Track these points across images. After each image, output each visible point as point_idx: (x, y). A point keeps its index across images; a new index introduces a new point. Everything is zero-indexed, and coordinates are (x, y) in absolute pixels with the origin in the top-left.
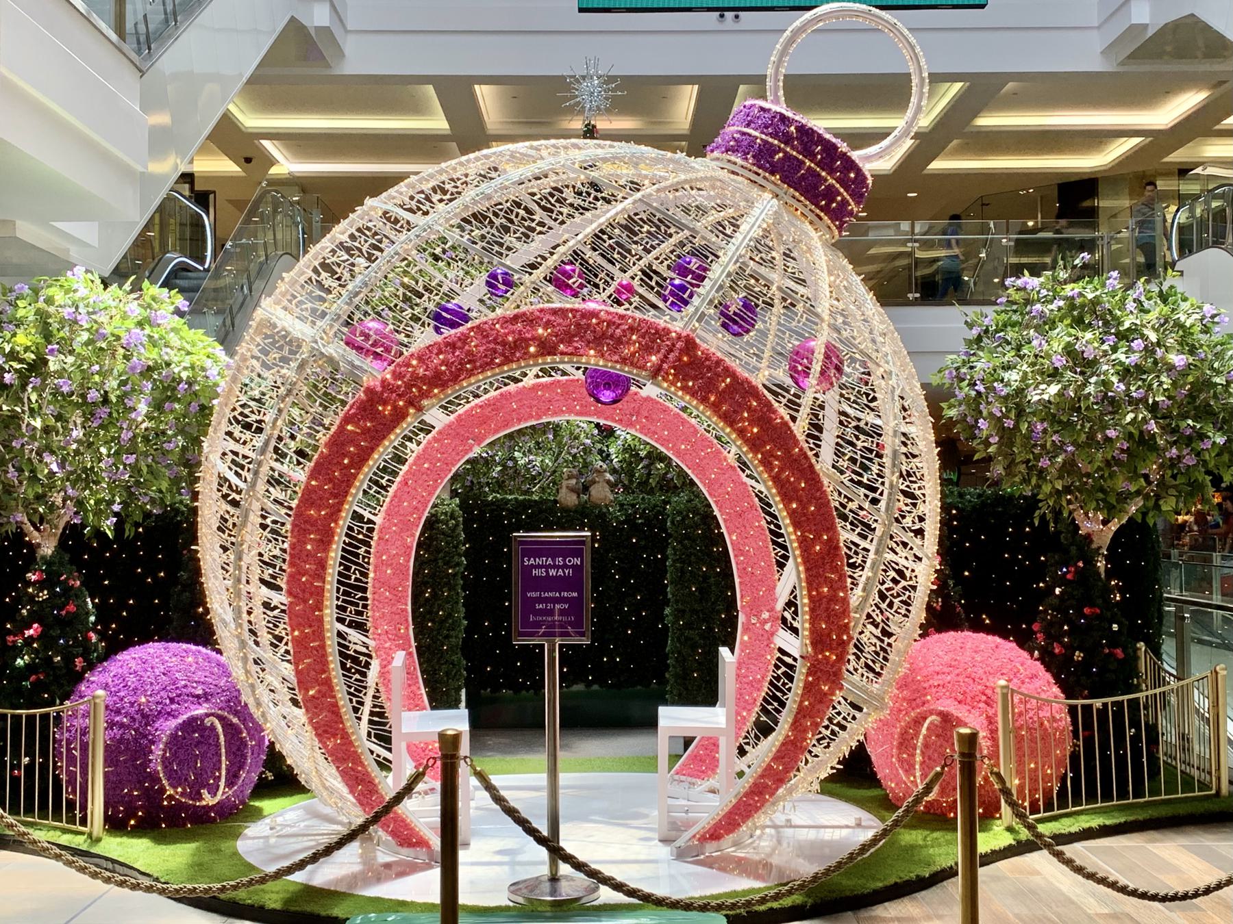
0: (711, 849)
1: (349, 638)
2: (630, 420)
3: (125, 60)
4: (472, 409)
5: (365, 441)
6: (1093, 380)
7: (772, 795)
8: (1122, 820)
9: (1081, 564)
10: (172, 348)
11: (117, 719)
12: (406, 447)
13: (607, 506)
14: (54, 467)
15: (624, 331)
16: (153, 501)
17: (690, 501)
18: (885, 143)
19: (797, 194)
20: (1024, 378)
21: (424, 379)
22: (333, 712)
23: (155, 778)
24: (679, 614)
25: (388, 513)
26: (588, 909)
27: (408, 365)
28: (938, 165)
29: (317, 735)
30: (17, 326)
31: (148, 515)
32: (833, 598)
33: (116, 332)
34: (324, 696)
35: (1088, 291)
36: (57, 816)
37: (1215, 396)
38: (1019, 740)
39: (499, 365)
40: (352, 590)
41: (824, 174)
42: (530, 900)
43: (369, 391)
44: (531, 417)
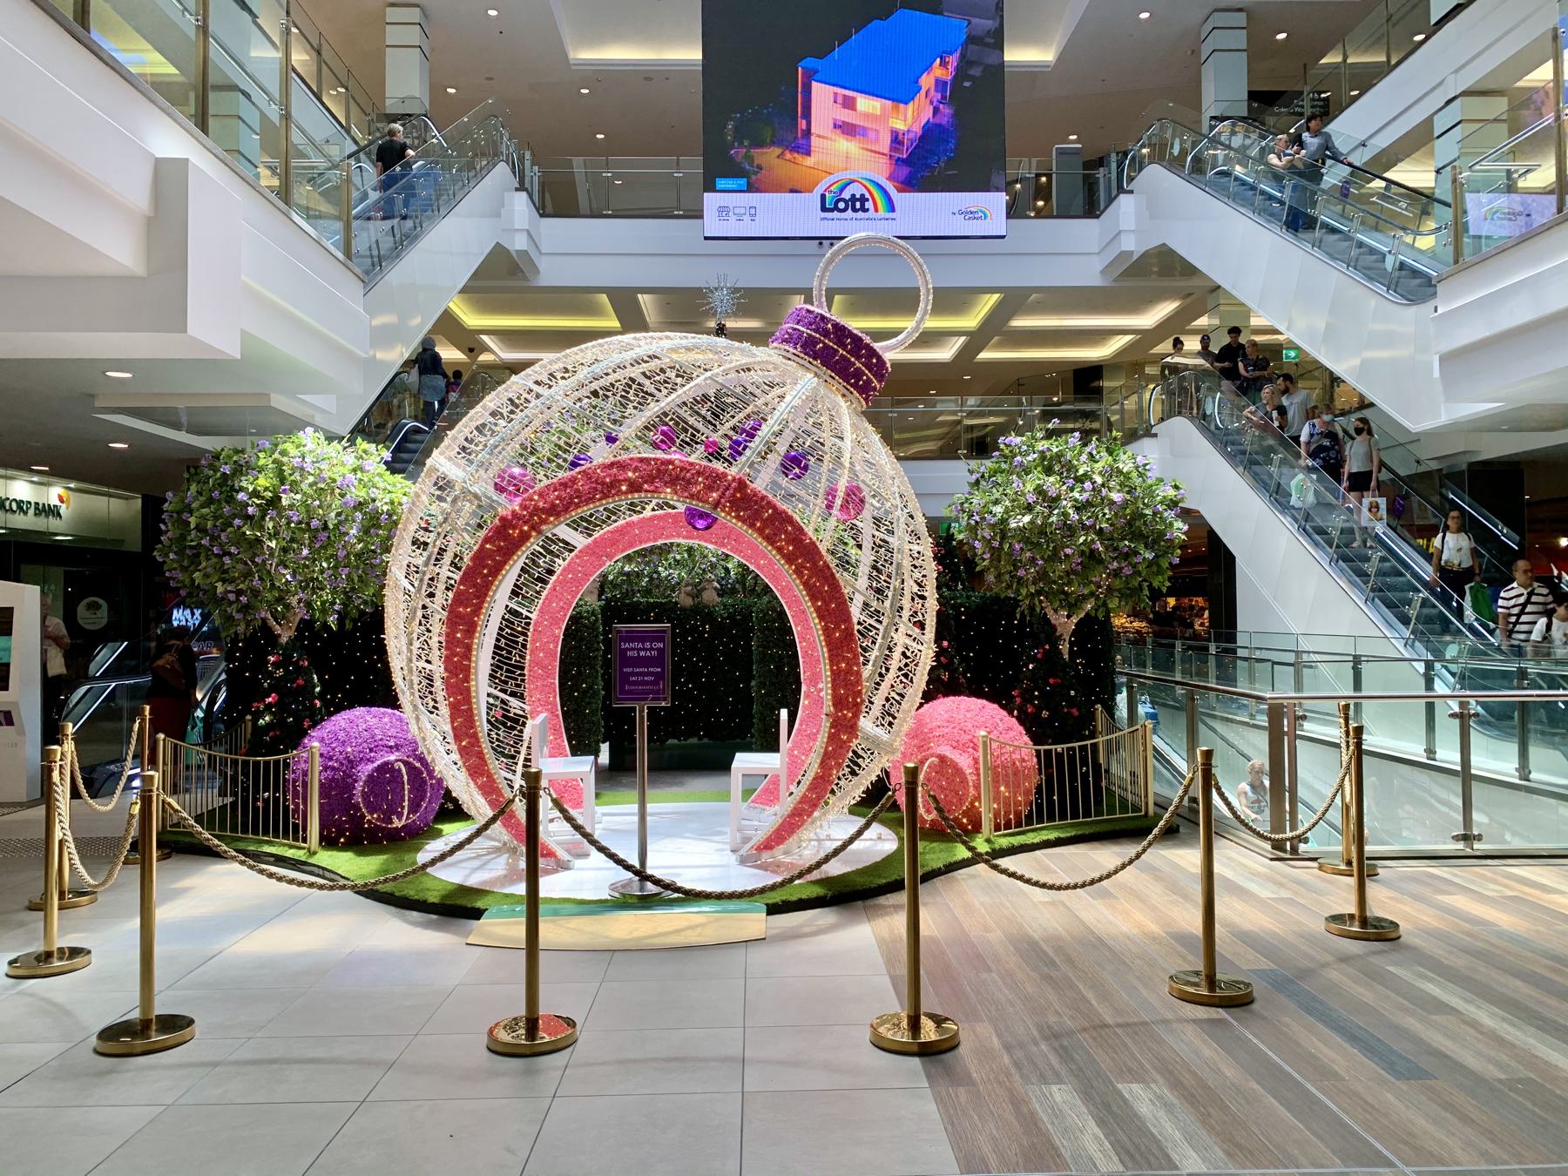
0: (766, 857)
1: (510, 704)
2: (723, 542)
3: (350, 274)
4: (605, 534)
5: (500, 556)
6: (1056, 512)
7: (809, 815)
8: (1073, 834)
9: (1047, 647)
10: (377, 488)
11: (330, 763)
12: (554, 562)
13: (713, 607)
14: (288, 577)
15: (693, 474)
16: (365, 602)
17: (769, 602)
18: (894, 341)
19: (833, 374)
20: (1007, 511)
21: (543, 510)
22: (480, 758)
23: (357, 807)
24: (762, 685)
25: (541, 611)
26: (665, 901)
27: (532, 500)
28: (984, 355)
29: (470, 775)
30: (259, 472)
31: (362, 613)
32: (849, 672)
33: (333, 476)
34: (473, 746)
35: (1054, 447)
36: (286, 836)
37: (1145, 522)
38: (996, 775)
39: (600, 500)
40: (508, 669)
41: (853, 359)
42: (623, 895)
43: (503, 519)
44: (649, 540)
